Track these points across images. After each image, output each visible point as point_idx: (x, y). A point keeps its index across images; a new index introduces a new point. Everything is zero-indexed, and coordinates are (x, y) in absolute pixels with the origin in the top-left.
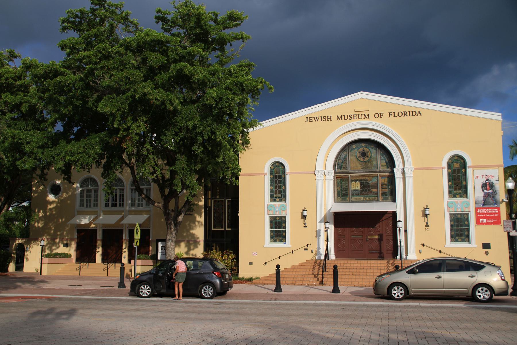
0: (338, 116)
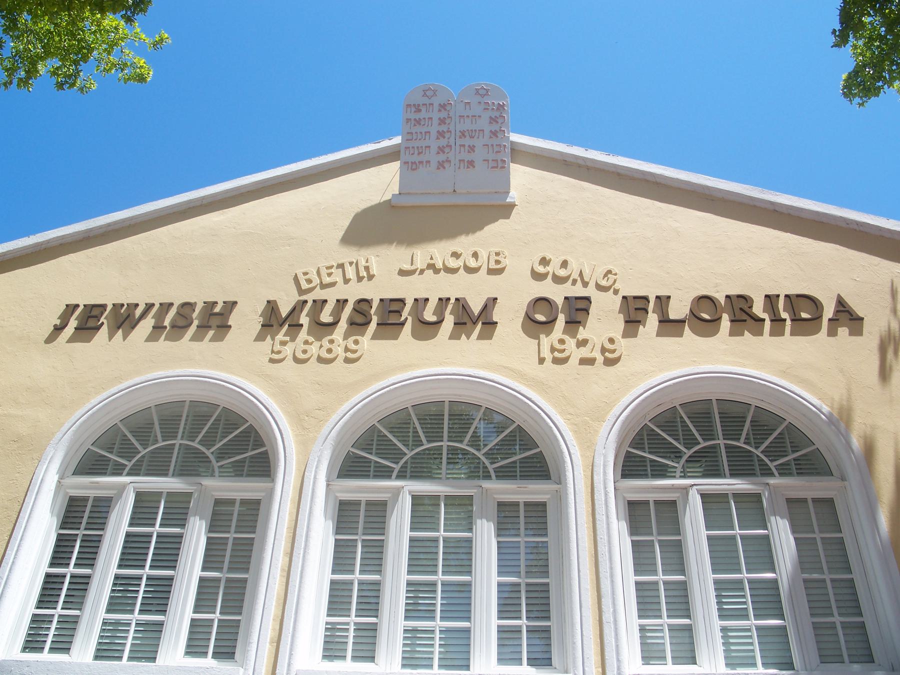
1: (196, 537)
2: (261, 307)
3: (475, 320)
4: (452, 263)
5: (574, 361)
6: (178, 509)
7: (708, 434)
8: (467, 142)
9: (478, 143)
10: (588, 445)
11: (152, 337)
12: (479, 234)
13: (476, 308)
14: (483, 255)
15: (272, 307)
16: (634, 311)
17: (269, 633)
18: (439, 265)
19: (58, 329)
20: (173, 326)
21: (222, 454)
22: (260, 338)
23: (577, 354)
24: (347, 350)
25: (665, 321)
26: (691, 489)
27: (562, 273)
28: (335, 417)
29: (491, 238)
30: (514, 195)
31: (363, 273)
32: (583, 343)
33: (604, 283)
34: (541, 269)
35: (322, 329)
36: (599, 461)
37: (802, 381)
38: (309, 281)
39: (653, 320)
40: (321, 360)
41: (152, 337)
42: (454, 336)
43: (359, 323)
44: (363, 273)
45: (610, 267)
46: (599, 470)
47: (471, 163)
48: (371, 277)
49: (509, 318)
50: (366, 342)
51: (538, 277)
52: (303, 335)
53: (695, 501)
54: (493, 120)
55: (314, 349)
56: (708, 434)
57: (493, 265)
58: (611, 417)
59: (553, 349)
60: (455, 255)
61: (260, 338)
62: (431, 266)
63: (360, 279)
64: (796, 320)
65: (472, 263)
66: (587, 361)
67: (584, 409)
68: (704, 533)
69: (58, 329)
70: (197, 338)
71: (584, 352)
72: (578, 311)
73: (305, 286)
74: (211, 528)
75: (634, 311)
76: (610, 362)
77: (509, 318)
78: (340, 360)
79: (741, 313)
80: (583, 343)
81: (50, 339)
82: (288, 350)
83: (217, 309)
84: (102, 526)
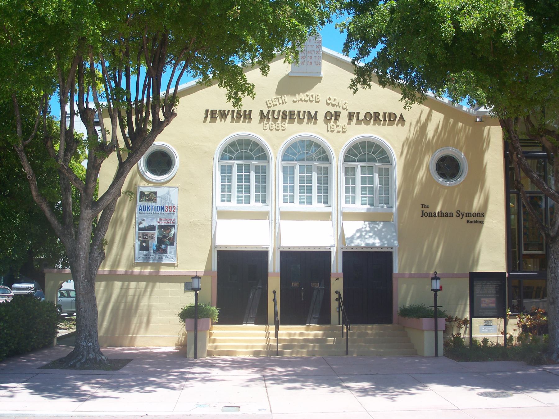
0: (262, 112)
1: (253, 175)
2: (259, 112)
3: (312, 118)
4: (307, 99)
5: (335, 131)
6: (248, 169)
7: (364, 151)
8: (310, 55)
9: (313, 55)
10: (338, 155)
11: (232, 122)
12: (312, 90)
13: (313, 115)
14: (314, 96)
15: (262, 112)
16: (351, 116)
17: (273, 198)
18: (303, 100)
19: (206, 117)
20: (237, 117)
21: (255, 154)
22: (260, 123)
23: (337, 129)
24: (282, 127)
25: (358, 119)
26: (359, 166)
27: (334, 103)
28: (281, 146)
29: (317, 91)
30: (322, 74)
31: (284, 101)
32: (338, 126)
33: (344, 107)
34: (329, 102)
35: (275, 120)
36: (340, 160)
37: (388, 140)
38: (270, 104)
39: (355, 119)
40: (276, 130)
41: (232, 122)
42: (308, 123)
43: (284, 118)
44: (284, 101)
45: (346, 101)
46: (339, 162)
47: (311, 63)
48: (286, 103)
49: (321, 117)
50: (286, 124)
51: (328, 104)
52: (271, 122)
53: (359, 168)
54: (317, 47)
55: (274, 126)
56: (364, 151)
57: (317, 100)
58: (343, 148)
59: (331, 128)
60: (307, 96)
61: (260, 123)
62: (301, 99)
63: (283, 103)
64: (389, 120)
65: (312, 99)
66: (339, 132)
67: (337, 141)
68: (360, 185)
69: (206, 117)
70: (244, 122)
71: (338, 129)
72: (337, 115)
73: (269, 105)
74: (256, 173)
75: (351, 116)
76: (344, 132)
77: (321, 117)
78: (281, 130)
79: (376, 117)
80: (338, 126)
81: (205, 121)
82: (268, 126)
83: (247, 113)
84: (231, 173)
